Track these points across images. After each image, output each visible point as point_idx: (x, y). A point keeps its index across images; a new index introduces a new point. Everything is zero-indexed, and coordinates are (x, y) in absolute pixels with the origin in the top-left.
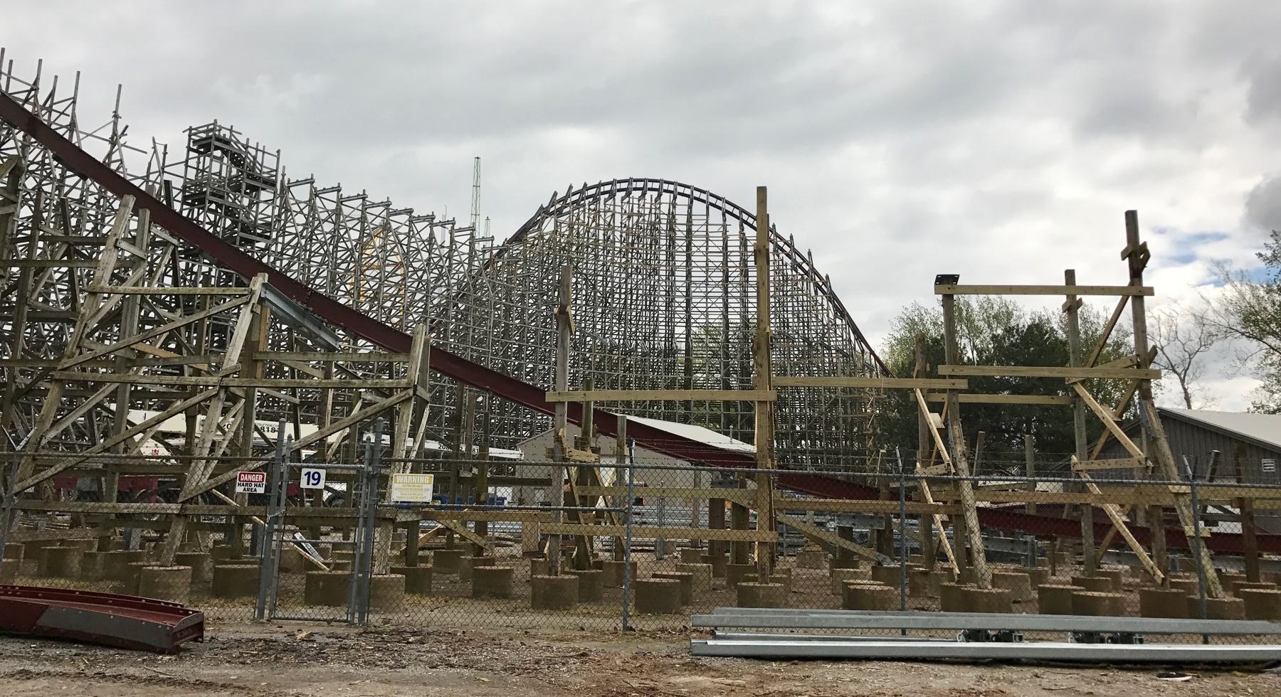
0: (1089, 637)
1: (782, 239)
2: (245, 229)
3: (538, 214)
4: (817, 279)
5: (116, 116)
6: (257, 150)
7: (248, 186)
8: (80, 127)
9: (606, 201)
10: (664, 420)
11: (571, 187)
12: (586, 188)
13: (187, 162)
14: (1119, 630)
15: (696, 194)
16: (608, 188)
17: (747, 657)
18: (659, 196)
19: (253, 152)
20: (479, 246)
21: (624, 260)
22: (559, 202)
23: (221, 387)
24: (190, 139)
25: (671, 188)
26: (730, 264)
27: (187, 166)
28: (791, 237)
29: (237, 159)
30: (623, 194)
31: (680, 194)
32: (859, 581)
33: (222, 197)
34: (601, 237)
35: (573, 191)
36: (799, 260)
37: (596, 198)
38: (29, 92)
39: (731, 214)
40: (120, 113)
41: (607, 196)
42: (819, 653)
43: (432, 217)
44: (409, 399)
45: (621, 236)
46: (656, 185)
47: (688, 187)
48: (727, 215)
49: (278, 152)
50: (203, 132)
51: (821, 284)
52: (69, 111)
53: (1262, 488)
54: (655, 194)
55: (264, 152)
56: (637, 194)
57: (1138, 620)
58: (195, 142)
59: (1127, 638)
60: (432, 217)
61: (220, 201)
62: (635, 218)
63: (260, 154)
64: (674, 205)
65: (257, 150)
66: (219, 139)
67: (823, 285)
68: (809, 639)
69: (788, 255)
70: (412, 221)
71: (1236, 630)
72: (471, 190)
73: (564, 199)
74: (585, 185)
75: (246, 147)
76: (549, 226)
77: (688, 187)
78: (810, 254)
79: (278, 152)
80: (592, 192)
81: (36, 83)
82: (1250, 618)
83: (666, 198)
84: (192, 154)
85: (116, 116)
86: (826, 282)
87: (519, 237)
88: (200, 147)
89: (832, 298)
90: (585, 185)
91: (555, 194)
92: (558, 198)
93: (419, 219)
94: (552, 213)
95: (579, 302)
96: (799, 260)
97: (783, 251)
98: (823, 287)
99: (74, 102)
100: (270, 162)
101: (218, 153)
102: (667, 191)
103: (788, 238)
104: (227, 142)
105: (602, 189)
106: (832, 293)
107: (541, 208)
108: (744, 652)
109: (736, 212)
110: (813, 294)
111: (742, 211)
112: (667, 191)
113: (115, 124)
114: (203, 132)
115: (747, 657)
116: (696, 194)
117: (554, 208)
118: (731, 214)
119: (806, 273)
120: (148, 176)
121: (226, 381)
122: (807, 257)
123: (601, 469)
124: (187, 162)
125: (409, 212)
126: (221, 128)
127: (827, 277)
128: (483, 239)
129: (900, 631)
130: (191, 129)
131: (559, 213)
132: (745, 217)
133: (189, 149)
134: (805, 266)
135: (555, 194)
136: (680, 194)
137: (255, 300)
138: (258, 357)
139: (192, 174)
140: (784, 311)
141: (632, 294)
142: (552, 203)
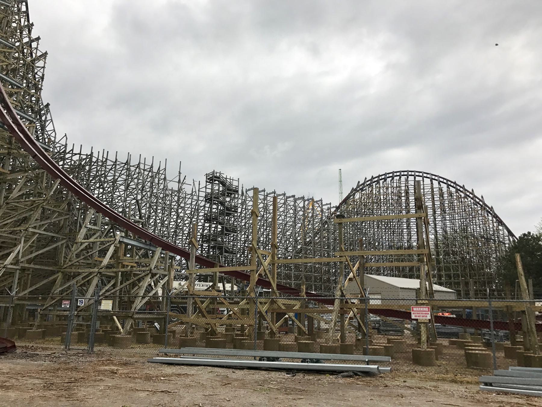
0: (304, 360)
1: (468, 191)
2: (228, 209)
3: (351, 192)
4: (488, 209)
5: (180, 173)
6: (230, 179)
7: (228, 193)
8: (167, 178)
9: (383, 182)
10: (409, 278)
11: (366, 178)
12: (373, 178)
13: (206, 186)
14: (314, 358)
15: (425, 175)
16: (383, 177)
17: (160, 363)
18: (400, 178)
19: (229, 180)
20: (325, 207)
21: (393, 207)
22: (361, 185)
23: (98, 272)
24: (206, 178)
25: (413, 173)
26: (436, 206)
27: (206, 188)
28: (473, 190)
29: (223, 183)
30: (391, 178)
31: (417, 176)
32: (480, 352)
33: (218, 198)
34: (382, 198)
35: (367, 180)
36: (478, 200)
37: (378, 182)
38: (150, 168)
39: (443, 182)
40: (181, 172)
41: (383, 180)
42: (185, 363)
43: (303, 198)
44: (148, 274)
45: (384, 197)
46: (406, 173)
47: (421, 172)
48: (441, 183)
49: (238, 179)
50: (211, 175)
51: (489, 210)
52: (164, 173)
53: (480, 301)
54: (398, 178)
55: (233, 180)
56: (403, 178)
57: (297, 353)
58: (208, 179)
59: (318, 361)
60: (303, 198)
61: (218, 200)
62: (398, 188)
63: (231, 181)
64: (407, 180)
65: (230, 179)
66: (216, 177)
67: (490, 211)
68: (185, 358)
69: (472, 199)
70: (295, 201)
71: (357, 359)
72: (338, 183)
73: (363, 184)
74: (372, 177)
75: (226, 179)
76: (357, 196)
77: (421, 172)
78: (482, 197)
79: (238, 179)
80: (376, 179)
81: (152, 165)
82: (341, 353)
83: (403, 178)
84: (208, 184)
85: (180, 173)
86: (492, 208)
87: (345, 201)
88: (210, 180)
89: (495, 216)
90: (372, 177)
91: (359, 182)
92: (360, 184)
93: (299, 199)
94: (358, 191)
95: (366, 227)
96: (478, 200)
97: (469, 197)
98: (491, 212)
99: (165, 170)
100: (235, 183)
101: (217, 182)
102: (403, 175)
103: (471, 191)
104: (219, 178)
105: (380, 178)
106: (495, 214)
107: (353, 189)
108: (161, 361)
109: (445, 181)
110: (486, 215)
111: (448, 180)
112: (403, 175)
113: (180, 176)
114: (211, 175)
115: (160, 363)
116: (425, 175)
117: (360, 188)
118: (443, 182)
119: (482, 206)
120: (192, 193)
121: (101, 271)
122: (481, 198)
123: (370, 300)
124: (206, 186)
125: (294, 196)
126: (217, 173)
127: (492, 207)
128: (327, 204)
129: (253, 358)
130: (207, 174)
131: (362, 190)
132: (449, 183)
133: (207, 182)
134: (481, 203)
135: (359, 182)
136: (417, 176)
137: (117, 242)
138: (120, 261)
139: (209, 191)
140: (454, 226)
141: (399, 222)
142: (358, 186)
